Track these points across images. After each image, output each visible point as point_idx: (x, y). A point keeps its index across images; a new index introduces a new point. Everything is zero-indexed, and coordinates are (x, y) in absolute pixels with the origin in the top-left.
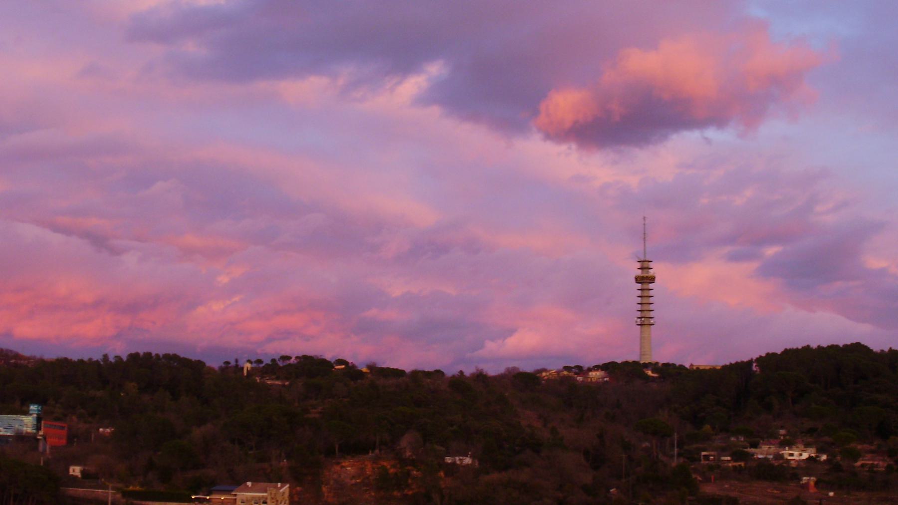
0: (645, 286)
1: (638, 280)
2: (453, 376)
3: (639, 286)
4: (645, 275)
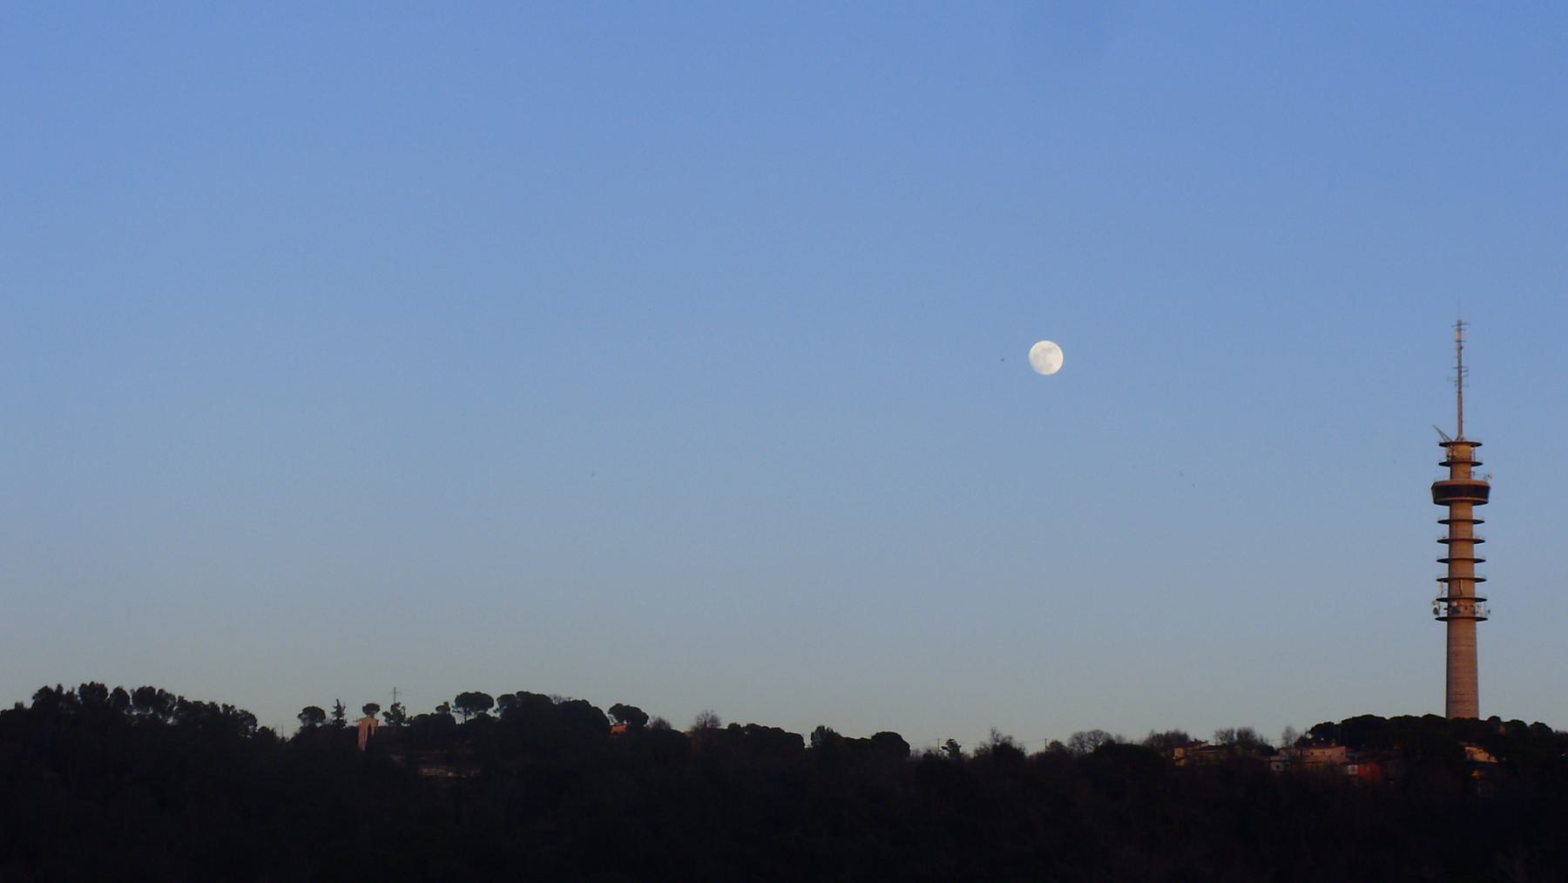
0: (1461, 512)
1: (1442, 493)
2: (422, 717)
3: (1444, 512)
4: (1462, 480)
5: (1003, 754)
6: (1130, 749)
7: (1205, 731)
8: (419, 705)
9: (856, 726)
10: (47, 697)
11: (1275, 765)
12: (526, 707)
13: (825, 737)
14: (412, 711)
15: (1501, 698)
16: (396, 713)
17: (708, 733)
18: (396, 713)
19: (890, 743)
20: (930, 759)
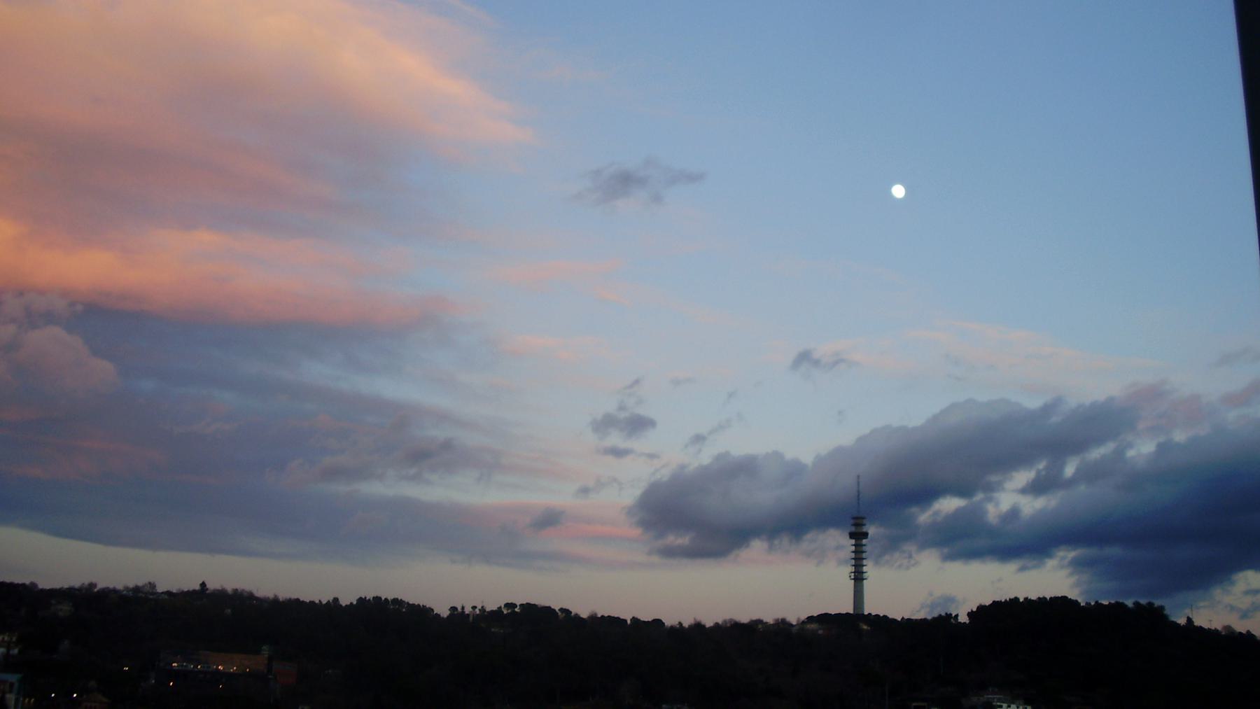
3: (853, 542)
4: (859, 530)
5: (698, 626)
6: (743, 625)
7: (769, 619)
8: (491, 606)
9: (646, 616)
10: (361, 600)
11: (794, 630)
12: (529, 608)
13: (634, 620)
14: (488, 609)
15: (872, 607)
16: (483, 609)
17: (593, 618)
18: (483, 609)
19: (658, 622)
20: (672, 627)
